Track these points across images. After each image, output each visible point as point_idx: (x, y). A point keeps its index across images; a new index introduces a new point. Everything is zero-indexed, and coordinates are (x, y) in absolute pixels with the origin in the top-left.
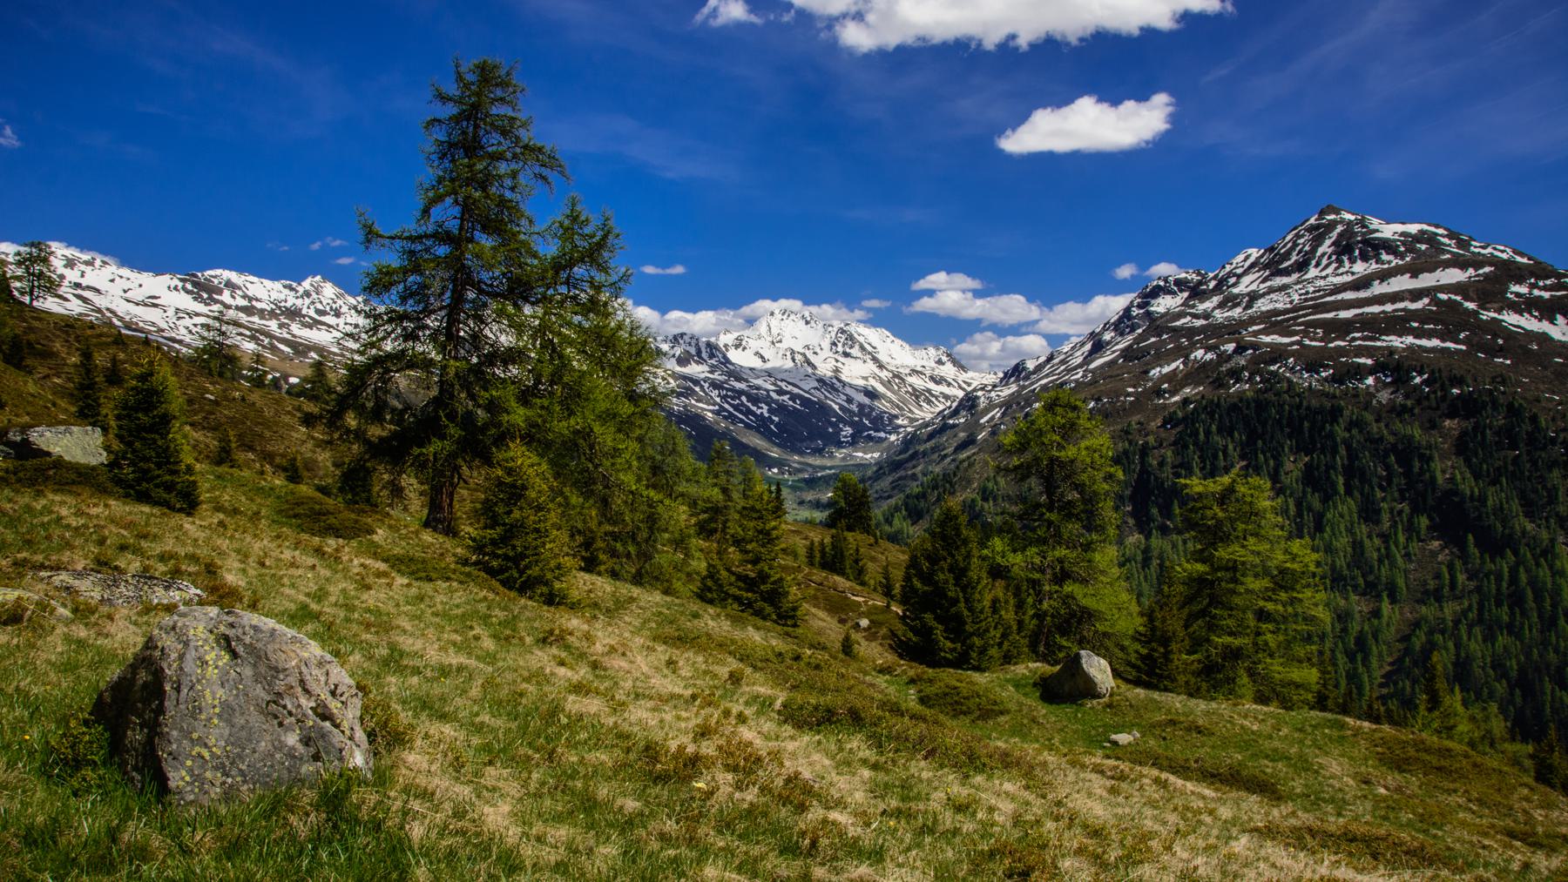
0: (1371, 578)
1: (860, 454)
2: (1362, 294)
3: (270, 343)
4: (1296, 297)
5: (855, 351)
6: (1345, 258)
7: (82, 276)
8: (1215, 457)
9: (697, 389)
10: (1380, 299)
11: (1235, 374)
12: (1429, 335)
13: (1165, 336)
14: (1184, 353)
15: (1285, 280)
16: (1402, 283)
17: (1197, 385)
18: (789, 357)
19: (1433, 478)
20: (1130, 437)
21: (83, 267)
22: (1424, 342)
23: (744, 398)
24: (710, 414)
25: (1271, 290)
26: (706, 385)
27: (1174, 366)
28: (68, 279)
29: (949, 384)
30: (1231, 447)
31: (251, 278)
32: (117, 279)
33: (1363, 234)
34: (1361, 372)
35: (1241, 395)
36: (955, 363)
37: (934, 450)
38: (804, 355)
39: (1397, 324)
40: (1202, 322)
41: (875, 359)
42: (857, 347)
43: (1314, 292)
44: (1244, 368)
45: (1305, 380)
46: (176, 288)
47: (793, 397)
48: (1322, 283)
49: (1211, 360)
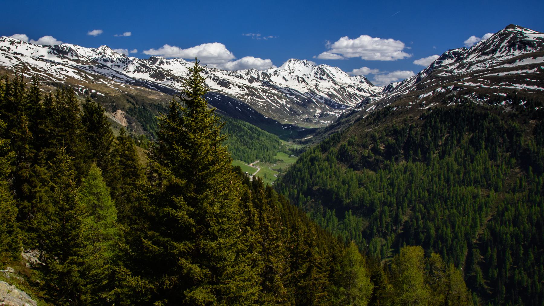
0: (489, 182)
1: (322, 121)
2: (512, 66)
3: (85, 76)
4: (488, 65)
5: (325, 77)
6: (512, 48)
7: (16, 48)
8: (437, 132)
9: (256, 93)
10: (517, 68)
11: (451, 98)
12: (533, 84)
13: (434, 80)
14: (433, 89)
15: (486, 57)
16: (529, 61)
17: (436, 102)
18: (296, 79)
19: (520, 144)
20: (406, 122)
21: (17, 44)
22: (531, 87)
23: (276, 97)
24: (261, 103)
25: (479, 62)
26: (260, 91)
27: (429, 94)
28: (11, 49)
29: (365, 92)
30: (443, 128)
31: (79, 47)
32: (29, 49)
33: (521, 38)
34: (501, 99)
35: (450, 108)
36: (368, 82)
37: (347, 121)
38: (303, 78)
39: (520, 79)
40: (449, 74)
41: (333, 81)
42: (326, 75)
43: (495, 63)
44: (454, 96)
45: (478, 101)
46: (50, 52)
47: (297, 96)
48: (500, 59)
49: (444, 92)
